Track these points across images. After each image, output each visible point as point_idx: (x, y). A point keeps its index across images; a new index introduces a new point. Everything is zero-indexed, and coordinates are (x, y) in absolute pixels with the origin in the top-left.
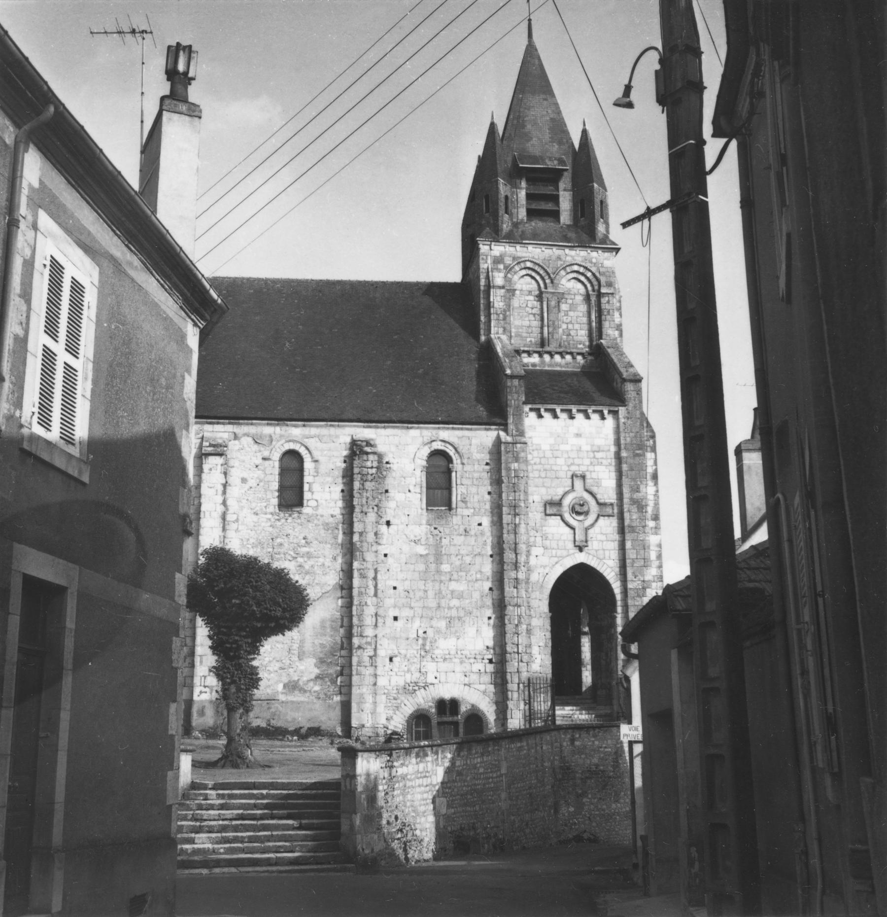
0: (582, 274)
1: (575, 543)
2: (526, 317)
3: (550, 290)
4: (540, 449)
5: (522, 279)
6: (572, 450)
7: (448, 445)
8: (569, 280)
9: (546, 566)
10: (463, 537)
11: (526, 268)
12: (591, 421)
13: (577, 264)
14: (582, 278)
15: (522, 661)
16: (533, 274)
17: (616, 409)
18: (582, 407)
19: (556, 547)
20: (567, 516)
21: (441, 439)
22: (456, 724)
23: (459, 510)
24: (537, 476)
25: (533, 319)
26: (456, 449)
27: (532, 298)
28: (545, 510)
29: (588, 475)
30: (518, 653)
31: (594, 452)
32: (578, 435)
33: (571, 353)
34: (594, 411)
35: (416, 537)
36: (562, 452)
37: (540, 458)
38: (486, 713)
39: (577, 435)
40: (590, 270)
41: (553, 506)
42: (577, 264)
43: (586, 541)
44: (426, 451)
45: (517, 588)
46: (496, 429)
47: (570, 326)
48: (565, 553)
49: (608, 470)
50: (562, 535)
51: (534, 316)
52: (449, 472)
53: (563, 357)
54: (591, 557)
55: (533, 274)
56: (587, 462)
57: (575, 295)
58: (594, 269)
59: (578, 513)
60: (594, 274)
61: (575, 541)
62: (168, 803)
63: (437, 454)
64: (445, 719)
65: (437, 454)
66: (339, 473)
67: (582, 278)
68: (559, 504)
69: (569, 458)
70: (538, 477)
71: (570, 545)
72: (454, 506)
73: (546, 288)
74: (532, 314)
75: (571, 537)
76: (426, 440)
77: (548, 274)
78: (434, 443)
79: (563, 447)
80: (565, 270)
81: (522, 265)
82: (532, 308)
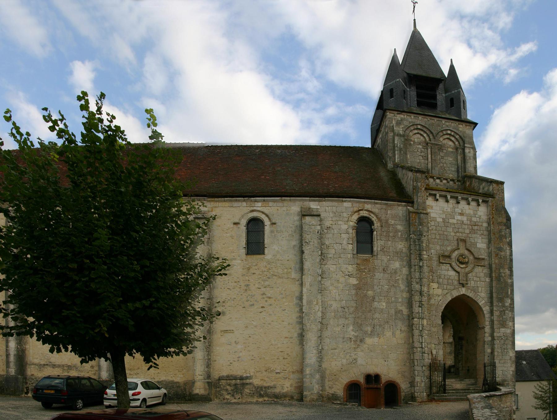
0: (453, 136)
1: (459, 281)
2: (417, 157)
3: (433, 142)
4: (436, 221)
5: (414, 136)
6: (457, 223)
7: (371, 214)
8: (444, 139)
9: (440, 295)
10: (382, 274)
11: (417, 129)
12: (470, 207)
13: (450, 130)
14: (453, 139)
15: (424, 353)
16: (422, 133)
17: (488, 200)
18: (465, 196)
19: (446, 283)
20: (454, 264)
21: (366, 209)
22: (378, 389)
23: (379, 256)
24: (434, 237)
25: (422, 159)
26: (377, 216)
27: (421, 147)
28: (439, 260)
29: (468, 239)
30: (422, 348)
31: (472, 226)
32: (461, 214)
33: (446, 179)
34: (473, 200)
35: (349, 272)
36: (451, 223)
37: (436, 227)
38: (399, 383)
39: (461, 214)
40: (458, 134)
41: (444, 258)
42: (450, 130)
43: (467, 281)
44: (355, 217)
45: (421, 307)
46: (405, 206)
47: (445, 165)
48: (452, 287)
49: (481, 238)
50: (450, 276)
51: (423, 157)
52: (372, 231)
53: (441, 181)
54: (469, 291)
55: (422, 133)
56: (467, 231)
57: (448, 147)
58: (460, 134)
59: (462, 263)
60: (460, 137)
61: (459, 280)
62: (188, 328)
63: (362, 220)
64: (371, 386)
65: (362, 220)
66: (231, 373)
67: (453, 139)
68: (449, 257)
69: (455, 228)
70: (435, 239)
71: (456, 283)
72: (375, 253)
73: (430, 140)
74: (421, 155)
75: (457, 278)
76: (356, 209)
77: (432, 133)
78: (361, 212)
79: (451, 221)
80: (443, 133)
81: (415, 127)
82: (421, 153)
